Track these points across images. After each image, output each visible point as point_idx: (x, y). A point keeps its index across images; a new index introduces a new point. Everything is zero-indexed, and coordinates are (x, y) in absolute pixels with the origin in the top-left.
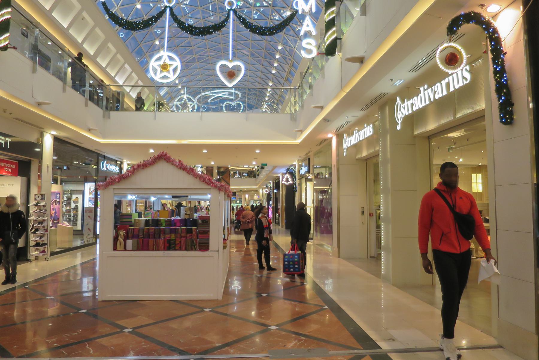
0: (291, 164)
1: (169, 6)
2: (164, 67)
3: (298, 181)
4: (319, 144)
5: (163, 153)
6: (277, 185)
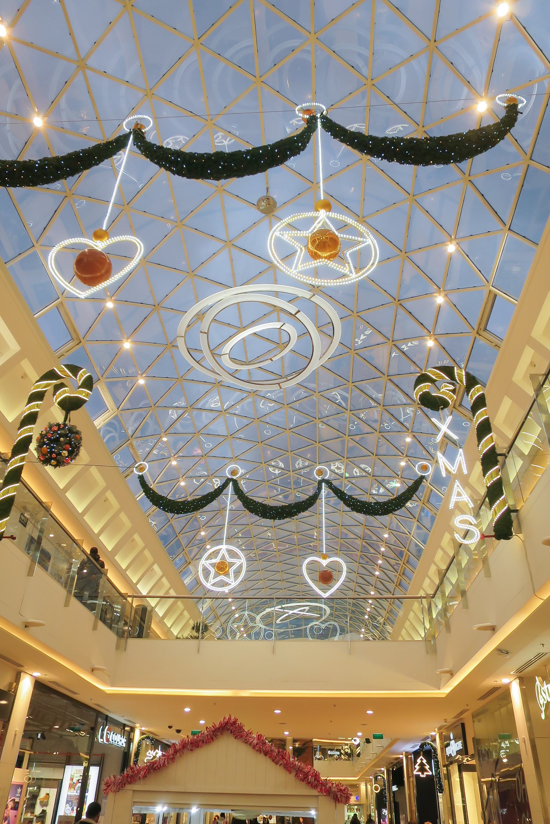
0: (426, 734)
1: (232, 480)
3: (444, 770)
4: (483, 697)
5: (230, 719)
6: (397, 775)
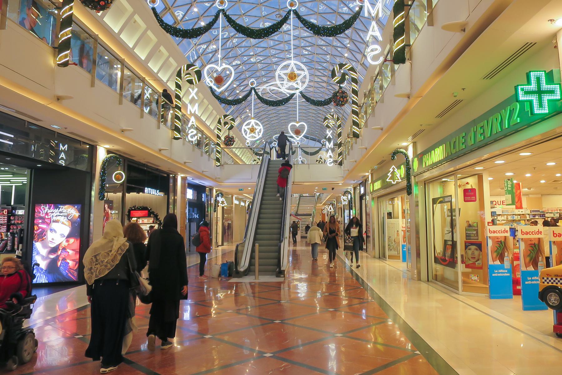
2: (252, 130)
